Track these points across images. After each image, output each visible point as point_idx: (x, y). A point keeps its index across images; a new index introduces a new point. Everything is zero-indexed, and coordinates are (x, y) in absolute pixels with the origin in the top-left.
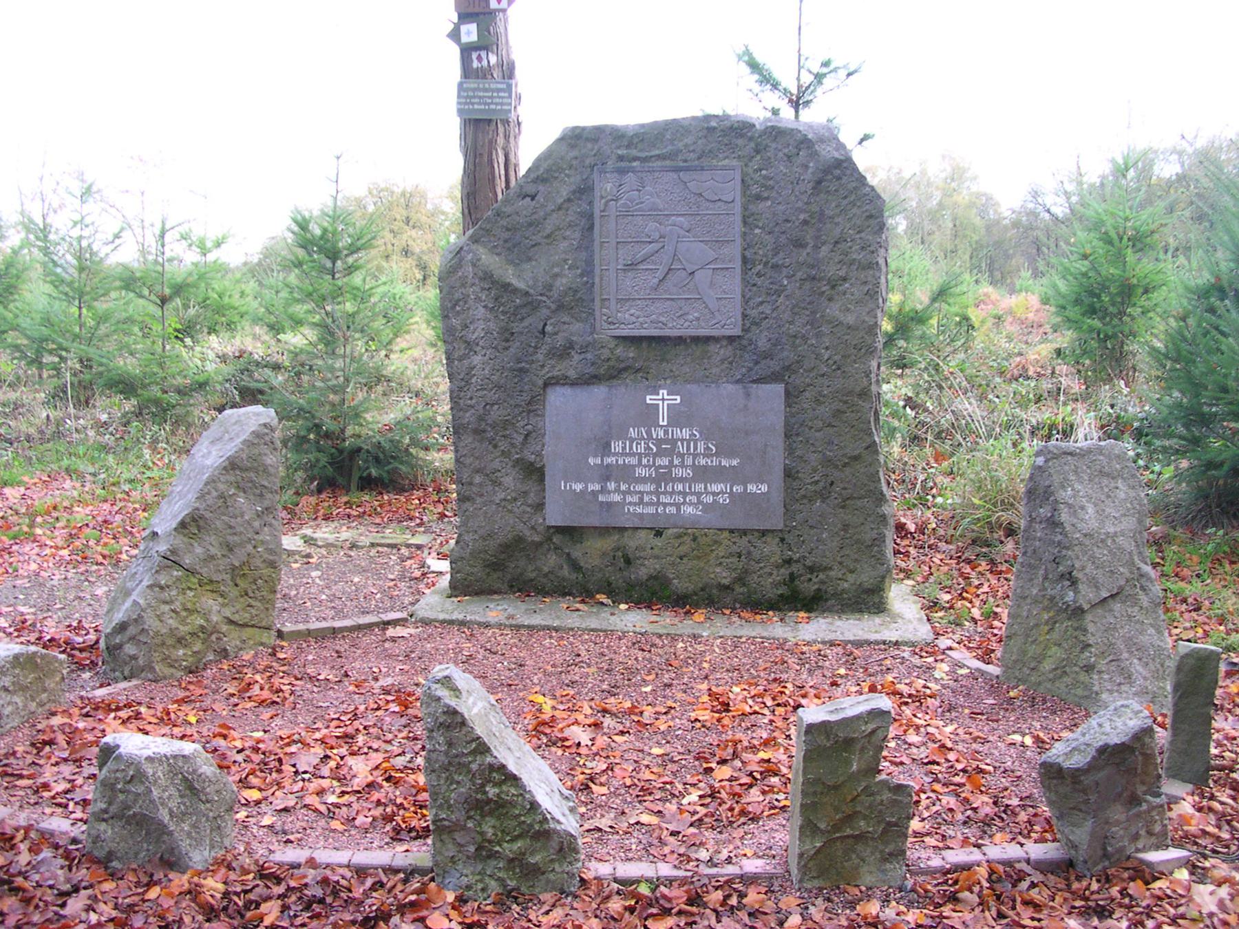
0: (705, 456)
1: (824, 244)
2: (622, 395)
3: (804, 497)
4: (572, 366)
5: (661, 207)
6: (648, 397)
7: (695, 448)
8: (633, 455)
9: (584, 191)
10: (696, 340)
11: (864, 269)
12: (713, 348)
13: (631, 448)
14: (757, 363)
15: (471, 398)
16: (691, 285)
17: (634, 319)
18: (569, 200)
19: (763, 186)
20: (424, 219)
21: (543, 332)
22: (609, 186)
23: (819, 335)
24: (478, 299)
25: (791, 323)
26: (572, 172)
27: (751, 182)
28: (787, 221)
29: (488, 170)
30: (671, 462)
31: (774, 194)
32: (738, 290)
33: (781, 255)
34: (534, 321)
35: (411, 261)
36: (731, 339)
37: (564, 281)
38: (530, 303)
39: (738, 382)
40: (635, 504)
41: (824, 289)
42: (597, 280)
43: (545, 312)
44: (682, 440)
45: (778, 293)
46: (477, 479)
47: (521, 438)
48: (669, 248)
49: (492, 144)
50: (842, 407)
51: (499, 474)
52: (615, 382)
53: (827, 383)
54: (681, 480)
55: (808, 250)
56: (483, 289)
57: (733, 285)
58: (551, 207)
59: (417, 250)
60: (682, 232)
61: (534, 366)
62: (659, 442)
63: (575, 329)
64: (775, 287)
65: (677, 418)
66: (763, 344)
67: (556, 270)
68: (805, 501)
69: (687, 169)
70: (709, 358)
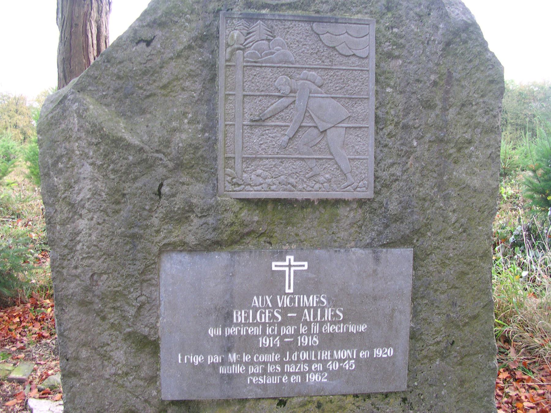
0: (332, 323)
1: (451, 106)
2: (246, 263)
3: (426, 357)
4: (192, 230)
5: (293, 59)
6: (274, 264)
7: (323, 316)
8: (257, 324)
9: (208, 38)
10: (324, 202)
11: (486, 132)
12: (342, 211)
13: (254, 317)
14: (387, 226)
15: (76, 267)
16: (323, 144)
17: (261, 180)
18: (190, 47)
19: (394, 44)
20: (24, 110)
21: (159, 194)
22: (236, 34)
23: (446, 198)
24: (84, 155)
25: (421, 185)
26: (193, 17)
27: (383, 40)
28: (418, 81)
29: (82, 39)
30: (297, 331)
31: (405, 53)
32: (371, 150)
33: (411, 115)
34: (148, 181)
35: (18, 131)
36: (361, 203)
37: (184, 136)
38: (146, 160)
39: (366, 246)
40: (258, 375)
41: (451, 151)
42: (220, 136)
43: (161, 171)
44: (309, 308)
45: (408, 154)
46: (84, 353)
47: (132, 311)
48: (301, 104)
49: (87, 15)
50: (466, 268)
51: (109, 348)
52: (237, 248)
53: (452, 246)
54: (307, 348)
55: (438, 111)
56: (90, 144)
57: (366, 145)
58: (168, 54)
59: (21, 126)
60: (314, 87)
61: (148, 231)
62: (284, 311)
63: (195, 191)
64: (405, 148)
65: (304, 285)
66: (393, 207)
67: (174, 124)
68: (426, 361)
69: (321, 20)
70: (338, 221)
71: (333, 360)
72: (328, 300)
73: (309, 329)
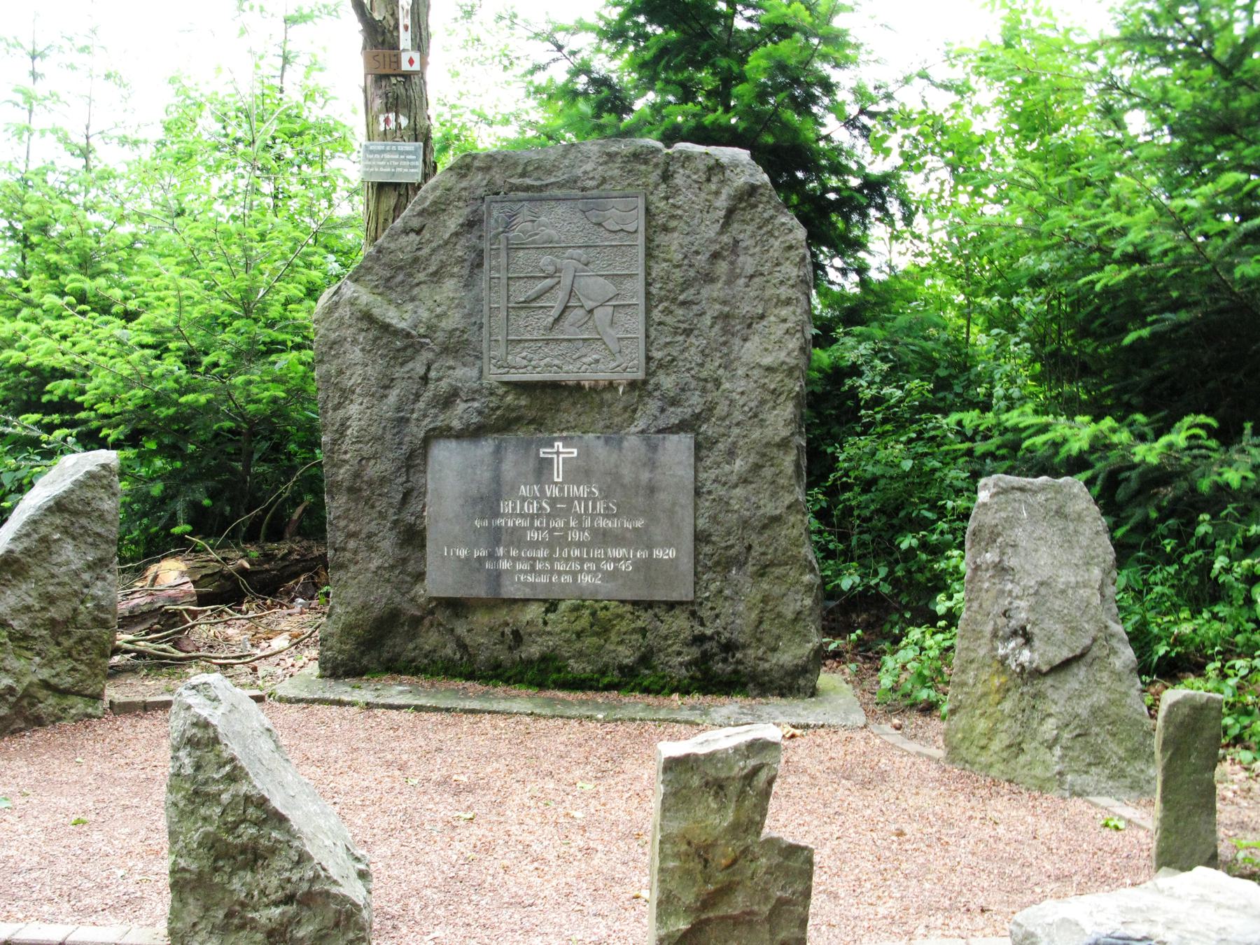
0: (606, 516)
7: (594, 508)
8: (522, 516)
13: (522, 508)
17: (525, 362)
24: (355, 342)
40: (525, 572)
48: (566, 281)
54: (580, 545)
62: (553, 501)
63: (463, 374)
71: (607, 559)
72: (600, 490)
73: (580, 523)
